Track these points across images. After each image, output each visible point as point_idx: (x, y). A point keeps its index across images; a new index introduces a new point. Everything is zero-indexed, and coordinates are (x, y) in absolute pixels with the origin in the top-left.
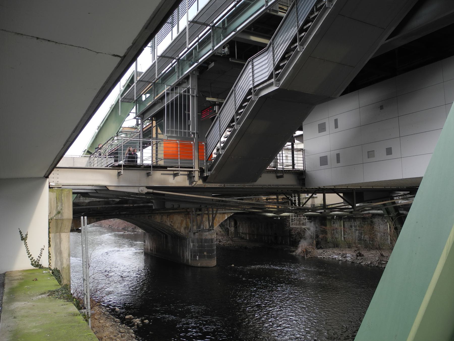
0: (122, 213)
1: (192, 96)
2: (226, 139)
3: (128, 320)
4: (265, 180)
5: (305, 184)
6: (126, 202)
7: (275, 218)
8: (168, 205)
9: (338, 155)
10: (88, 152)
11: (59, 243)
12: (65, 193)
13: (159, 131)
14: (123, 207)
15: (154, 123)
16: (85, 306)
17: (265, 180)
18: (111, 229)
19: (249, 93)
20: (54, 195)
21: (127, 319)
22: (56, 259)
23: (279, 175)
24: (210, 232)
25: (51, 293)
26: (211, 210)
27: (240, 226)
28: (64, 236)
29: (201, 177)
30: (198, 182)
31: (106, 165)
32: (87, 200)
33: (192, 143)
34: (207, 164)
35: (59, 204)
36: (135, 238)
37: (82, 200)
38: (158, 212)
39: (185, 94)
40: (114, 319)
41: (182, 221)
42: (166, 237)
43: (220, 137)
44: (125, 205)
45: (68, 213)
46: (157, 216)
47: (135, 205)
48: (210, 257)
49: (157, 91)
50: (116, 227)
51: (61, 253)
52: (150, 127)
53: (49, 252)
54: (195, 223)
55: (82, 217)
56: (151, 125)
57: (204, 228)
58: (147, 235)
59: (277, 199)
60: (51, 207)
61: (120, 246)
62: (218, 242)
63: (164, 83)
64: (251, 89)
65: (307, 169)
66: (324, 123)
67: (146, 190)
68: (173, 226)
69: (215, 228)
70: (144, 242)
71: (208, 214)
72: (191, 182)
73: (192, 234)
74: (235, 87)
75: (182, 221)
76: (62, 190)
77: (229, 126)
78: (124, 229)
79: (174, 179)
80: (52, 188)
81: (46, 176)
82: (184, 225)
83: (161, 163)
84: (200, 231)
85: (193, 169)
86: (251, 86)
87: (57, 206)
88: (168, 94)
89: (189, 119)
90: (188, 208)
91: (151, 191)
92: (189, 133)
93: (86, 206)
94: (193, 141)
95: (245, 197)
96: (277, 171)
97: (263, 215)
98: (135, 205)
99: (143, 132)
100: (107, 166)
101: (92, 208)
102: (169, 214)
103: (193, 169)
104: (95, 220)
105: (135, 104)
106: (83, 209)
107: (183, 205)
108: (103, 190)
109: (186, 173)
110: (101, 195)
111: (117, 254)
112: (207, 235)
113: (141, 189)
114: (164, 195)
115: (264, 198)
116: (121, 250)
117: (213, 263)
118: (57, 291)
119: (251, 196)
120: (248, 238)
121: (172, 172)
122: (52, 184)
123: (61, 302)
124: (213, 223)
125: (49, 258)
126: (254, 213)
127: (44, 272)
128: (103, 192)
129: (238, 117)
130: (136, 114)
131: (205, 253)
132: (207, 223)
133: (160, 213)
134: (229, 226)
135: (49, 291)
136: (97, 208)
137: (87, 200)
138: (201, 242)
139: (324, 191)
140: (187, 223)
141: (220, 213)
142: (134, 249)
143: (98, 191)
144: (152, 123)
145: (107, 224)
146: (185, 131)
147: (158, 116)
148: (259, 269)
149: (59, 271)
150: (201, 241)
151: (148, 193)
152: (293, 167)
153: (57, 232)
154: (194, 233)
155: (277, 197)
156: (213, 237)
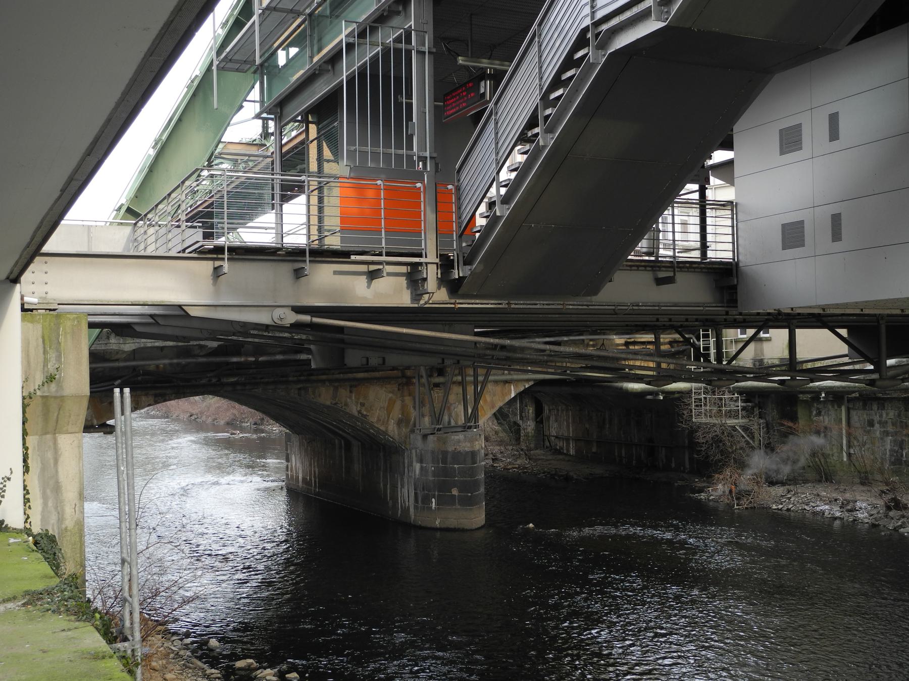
0: (225, 380)
1: (418, 52)
3: (243, 673)
4: (624, 290)
5: (736, 301)
7: (649, 397)
8: (354, 358)
9: (836, 219)
10: (129, 210)
11: (52, 462)
13: (327, 153)
14: (228, 364)
15: (313, 129)
16: (127, 632)
17: (624, 290)
18: (195, 424)
19: (581, 41)
20: (36, 330)
21: (240, 669)
22: (45, 504)
23: (662, 275)
24: (469, 433)
25: (33, 598)
27: (552, 419)
29: (445, 281)
30: (437, 295)
32: (129, 345)
33: (419, 185)
35: (52, 355)
37: (114, 343)
38: (324, 377)
39: (399, 46)
41: (391, 403)
42: (348, 446)
43: (497, 169)
44: (235, 359)
45: (77, 380)
46: (323, 390)
47: (260, 359)
48: (468, 502)
49: (320, 40)
50: (210, 420)
51: (57, 488)
52: (302, 143)
55: (117, 391)
56: (303, 136)
57: (453, 423)
58: (295, 439)
59: (657, 343)
60: (29, 363)
61: (221, 469)
63: (337, 17)
64: (585, 30)
65: (744, 260)
67: (292, 318)
68: (365, 416)
69: (481, 423)
70: (288, 460)
71: (463, 384)
72: (416, 297)
73: (419, 438)
74: (540, 24)
75: (391, 403)
76: (58, 316)
77: (522, 139)
79: (369, 287)
80: (31, 310)
82: (396, 413)
83: (334, 242)
84: (439, 430)
85: (422, 260)
86: (588, 22)
87: (46, 362)
88: (350, 46)
89: (410, 117)
90: (408, 368)
91: (306, 318)
92: (409, 157)
93: (126, 360)
94: (422, 181)
95: (565, 339)
96: (656, 265)
97: (617, 388)
98: (253, 359)
99: (282, 155)
100: (184, 251)
101: (143, 366)
103: (422, 260)
104: (151, 399)
105: (257, 76)
106: (118, 368)
109: (404, 269)
113: (278, 313)
114: (341, 329)
115: (619, 340)
117: (477, 517)
118: (49, 593)
120: (572, 452)
121: (364, 268)
122: (30, 299)
123: (61, 621)
124: (475, 409)
127: (12, 540)
129: (548, 112)
131: (455, 492)
132: (461, 408)
135: (27, 593)
137: (129, 345)
138: (444, 461)
139: (793, 320)
143: (160, 321)
145: (184, 412)
147: (325, 110)
149: (52, 539)
150: (443, 457)
151: (297, 326)
153: (46, 433)
156: (477, 447)
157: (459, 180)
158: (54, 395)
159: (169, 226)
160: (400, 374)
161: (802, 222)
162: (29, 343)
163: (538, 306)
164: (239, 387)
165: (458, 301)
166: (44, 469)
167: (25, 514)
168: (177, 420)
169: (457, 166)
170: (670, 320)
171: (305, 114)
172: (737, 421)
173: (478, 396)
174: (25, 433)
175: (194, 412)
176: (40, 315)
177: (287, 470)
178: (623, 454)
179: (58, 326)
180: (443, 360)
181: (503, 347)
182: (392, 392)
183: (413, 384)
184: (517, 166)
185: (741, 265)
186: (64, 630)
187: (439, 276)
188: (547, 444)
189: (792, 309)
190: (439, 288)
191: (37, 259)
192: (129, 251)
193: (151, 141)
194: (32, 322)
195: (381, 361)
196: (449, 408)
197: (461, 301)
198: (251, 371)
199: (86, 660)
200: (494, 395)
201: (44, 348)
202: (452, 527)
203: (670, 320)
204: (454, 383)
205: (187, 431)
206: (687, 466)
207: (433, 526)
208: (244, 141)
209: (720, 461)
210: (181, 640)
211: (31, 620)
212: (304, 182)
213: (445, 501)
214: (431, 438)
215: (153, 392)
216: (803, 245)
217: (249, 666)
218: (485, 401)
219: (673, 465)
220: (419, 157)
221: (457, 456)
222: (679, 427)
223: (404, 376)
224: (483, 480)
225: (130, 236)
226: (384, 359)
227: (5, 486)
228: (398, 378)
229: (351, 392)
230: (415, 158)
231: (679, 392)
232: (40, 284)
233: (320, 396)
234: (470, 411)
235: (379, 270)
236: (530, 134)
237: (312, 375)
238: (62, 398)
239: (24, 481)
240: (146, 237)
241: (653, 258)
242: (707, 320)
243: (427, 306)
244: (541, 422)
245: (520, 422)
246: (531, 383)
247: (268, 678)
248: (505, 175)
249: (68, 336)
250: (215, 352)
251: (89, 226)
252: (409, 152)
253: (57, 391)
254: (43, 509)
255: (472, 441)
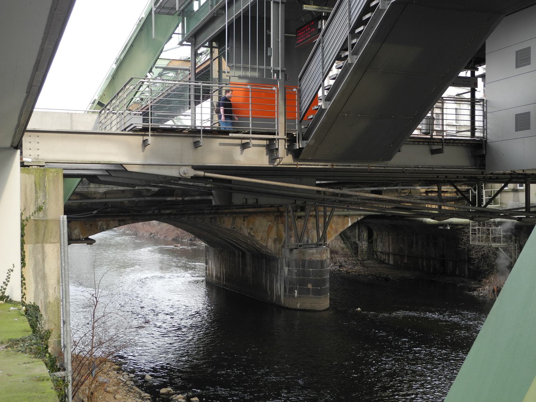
0: (163, 212)
2: (334, 81)
3: (165, 396)
4: (406, 158)
6: (171, 192)
7: (441, 227)
8: (238, 199)
11: (41, 260)
12: (51, 175)
14: (165, 201)
16: (65, 366)
17: (406, 158)
18: (153, 240)
20: (30, 179)
21: (163, 394)
22: (37, 287)
23: (435, 147)
24: (320, 249)
25: (13, 343)
26: (322, 209)
27: (379, 240)
28: (52, 250)
29: (290, 149)
30: (286, 159)
31: (123, 128)
32: (103, 189)
34: (300, 128)
35: (41, 194)
36: (193, 255)
38: (226, 211)
40: (140, 394)
41: (270, 228)
42: (244, 255)
43: (324, 77)
44: (169, 199)
46: (226, 219)
47: (185, 199)
48: (318, 293)
50: (162, 237)
51: (44, 277)
53: (22, 276)
54: (293, 233)
57: (310, 242)
58: (211, 250)
60: (26, 199)
62: (338, 268)
65: (491, 137)
66: (528, 50)
67: (192, 173)
68: (253, 236)
69: (328, 242)
70: (207, 263)
71: (316, 217)
72: (272, 160)
73: (288, 251)
75: (270, 228)
76: (44, 170)
77: (339, 58)
78: (176, 240)
79: (242, 153)
80: (29, 166)
81: (15, 145)
82: (273, 235)
84: (300, 246)
85: (275, 137)
87: (37, 198)
89: (268, 45)
90: (281, 206)
91: (201, 173)
92: (268, 71)
93: (100, 198)
95: (385, 188)
96: (430, 142)
97: (419, 221)
98: (181, 199)
100: (125, 129)
101: (98, 205)
102: (246, 216)
103: (275, 137)
106: (96, 203)
107: (263, 200)
108: (116, 173)
109: (264, 142)
110: (120, 180)
111: (160, 282)
112: (314, 254)
113: (183, 169)
114: (230, 181)
115: (423, 190)
116: (168, 275)
117: (324, 303)
118: (23, 340)
119: (396, 186)
120: (391, 262)
121: (239, 142)
123: (25, 357)
124: (324, 232)
125: (22, 286)
126: (402, 217)
127: (12, 308)
128: (120, 175)
129: (354, 41)
130: (183, 36)
131: (310, 286)
132: (315, 232)
133: (231, 213)
134: (359, 239)
135: (10, 340)
136: (122, 203)
137: (103, 189)
138: (303, 266)
140: (278, 231)
141: (339, 216)
142: (189, 275)
143: (112, 174)
144: (212, 52)
145: (147, 232)
146: (262, 67)
148: (405, 317)
149: (36, 308)
150: (302, 263)
151: (195, 178)
152: (473, 134)
153: (38, 243)
154: (291, 250)
155: (439, 189)
156: (324, 258)
157: (300, 86)
158: (41, 219)
159: (118, 114)
160: (276, 210)
161: (528, 113)
162: (26, 186)
163: (351, 167)
164: (172, 217)
165: (299, 163)
166: (36, 265)
167: (22, 292)
168: (142, 237)
169: (299, 77)
170: (446, 177)
171: (211, 41)
172: (499, 244)
173: (326, 225)
174: (23, 243)
175: (153, 232)
176: (33, 169)
177: (206, 270)
178: (425, 265)
179: (44, 176)
180: (295, 201)
181: (337, 195)
182: (271, 222)
183: (284, 216)
184: (335, 76)
185: (488, 141)
186: (25, 363)
187: (286, 147)
188: (375, 256)
189: (523, 171)
190: (287, 155)
191: (26, 133)
192: (96, 130)
193: (114, 60)
194: (28, 174)
195: (255, 201)
196: (308, 233)
197: (301, 163)
198: (180, 206)
199: (32, 381)
200: (338, 224)
201: (36, 190)
202: (308, 308)
203: (446, 177)
204: (311, 216)
205: (148, 245)
206: (467, 273)
207: (296, 308)
208: (183, 59)
209: (487, 271)
210: (128, 375)
211: (8, 356)
212: (200, 86)
213: (303, 292)
214: (295, 251)
215: (117, 218)
216: (529, 128)
217: (169, 392)
218: (332, 228)
219: (457, 273)
220: (274, 70)
221: (312, 263)
222: (460, 247)
223: (278, 211)
224: (328, 279)
225: (97, 120)
226: (257, 200)
227: (10, 275)
228: (274, 212)
229: (244, 220)
230: (272, 71)
231: (461, 225)
232: (33, 150)
233: (224, 223)
234: (321, 234)
235: (248, 143)
236: (343, 56)
237: (219, 209)
238: (47, 221)
239: (22, 272)
240: (106, 120)
241: (429, 137)
242: (471, 177)
243: (279, 166)
244: (372, 242)
245: (358, 242)
246: (362, 217)
247: (179, 400)
248: (329, 82)
249: (51, 182)
250: (156, 194)
251: (71, 114)
252: (268, 67)
253: (43, 217)
254: (35, 289)
255: (321, 253)
